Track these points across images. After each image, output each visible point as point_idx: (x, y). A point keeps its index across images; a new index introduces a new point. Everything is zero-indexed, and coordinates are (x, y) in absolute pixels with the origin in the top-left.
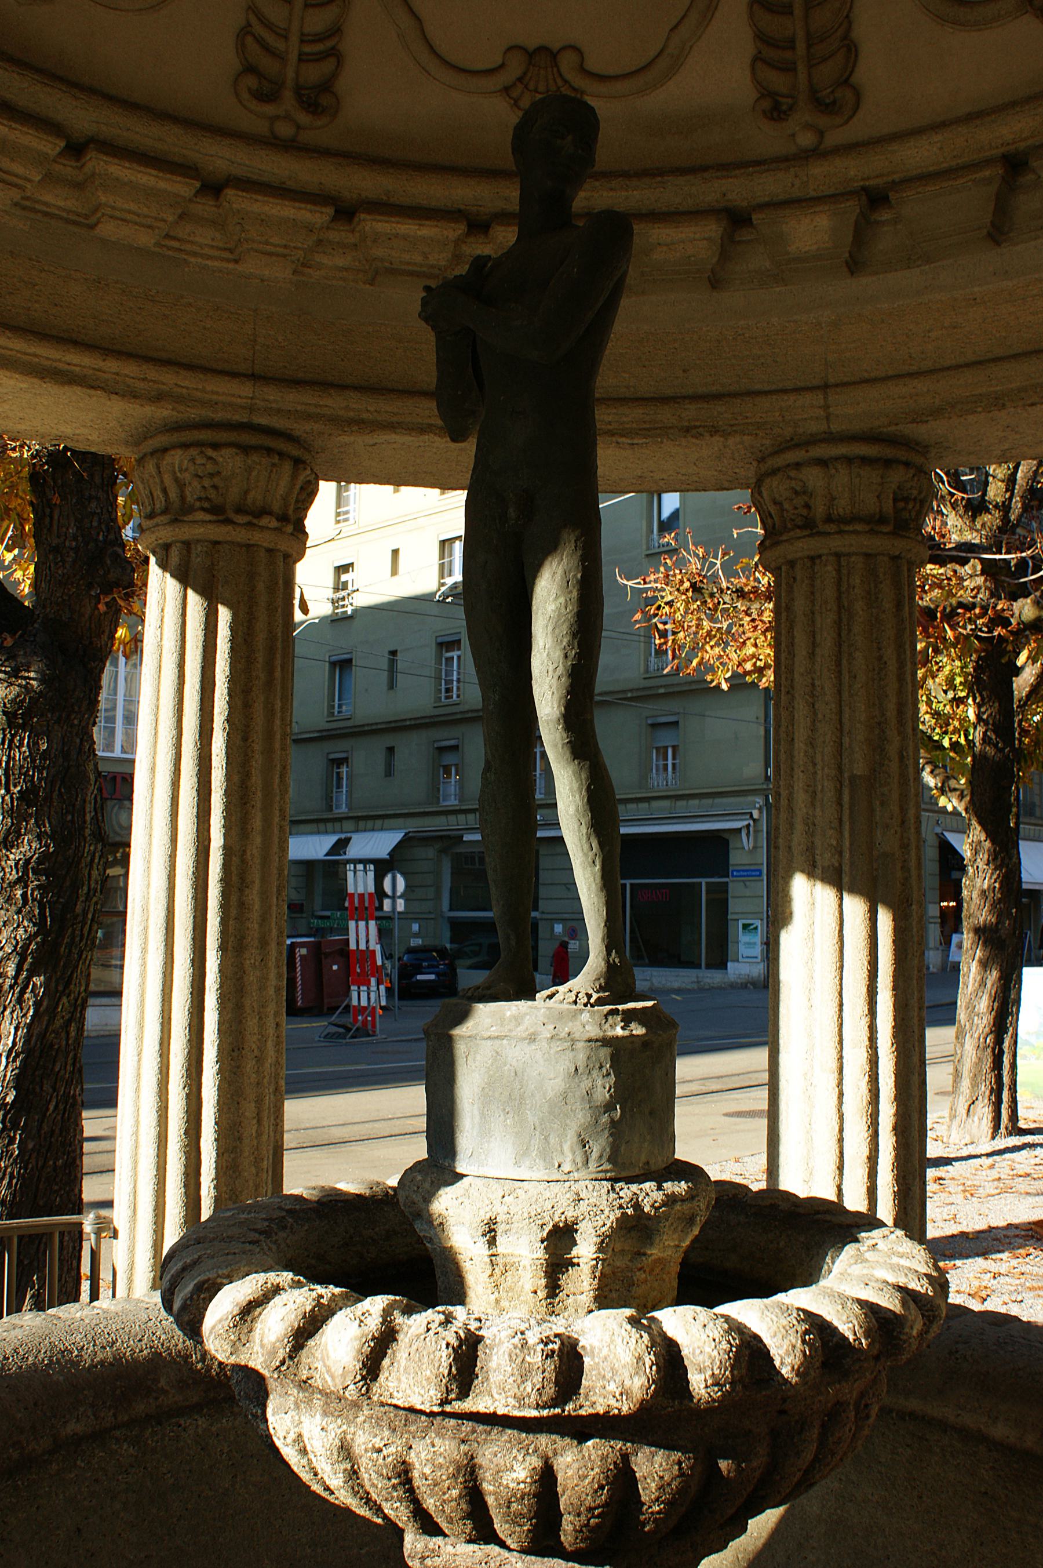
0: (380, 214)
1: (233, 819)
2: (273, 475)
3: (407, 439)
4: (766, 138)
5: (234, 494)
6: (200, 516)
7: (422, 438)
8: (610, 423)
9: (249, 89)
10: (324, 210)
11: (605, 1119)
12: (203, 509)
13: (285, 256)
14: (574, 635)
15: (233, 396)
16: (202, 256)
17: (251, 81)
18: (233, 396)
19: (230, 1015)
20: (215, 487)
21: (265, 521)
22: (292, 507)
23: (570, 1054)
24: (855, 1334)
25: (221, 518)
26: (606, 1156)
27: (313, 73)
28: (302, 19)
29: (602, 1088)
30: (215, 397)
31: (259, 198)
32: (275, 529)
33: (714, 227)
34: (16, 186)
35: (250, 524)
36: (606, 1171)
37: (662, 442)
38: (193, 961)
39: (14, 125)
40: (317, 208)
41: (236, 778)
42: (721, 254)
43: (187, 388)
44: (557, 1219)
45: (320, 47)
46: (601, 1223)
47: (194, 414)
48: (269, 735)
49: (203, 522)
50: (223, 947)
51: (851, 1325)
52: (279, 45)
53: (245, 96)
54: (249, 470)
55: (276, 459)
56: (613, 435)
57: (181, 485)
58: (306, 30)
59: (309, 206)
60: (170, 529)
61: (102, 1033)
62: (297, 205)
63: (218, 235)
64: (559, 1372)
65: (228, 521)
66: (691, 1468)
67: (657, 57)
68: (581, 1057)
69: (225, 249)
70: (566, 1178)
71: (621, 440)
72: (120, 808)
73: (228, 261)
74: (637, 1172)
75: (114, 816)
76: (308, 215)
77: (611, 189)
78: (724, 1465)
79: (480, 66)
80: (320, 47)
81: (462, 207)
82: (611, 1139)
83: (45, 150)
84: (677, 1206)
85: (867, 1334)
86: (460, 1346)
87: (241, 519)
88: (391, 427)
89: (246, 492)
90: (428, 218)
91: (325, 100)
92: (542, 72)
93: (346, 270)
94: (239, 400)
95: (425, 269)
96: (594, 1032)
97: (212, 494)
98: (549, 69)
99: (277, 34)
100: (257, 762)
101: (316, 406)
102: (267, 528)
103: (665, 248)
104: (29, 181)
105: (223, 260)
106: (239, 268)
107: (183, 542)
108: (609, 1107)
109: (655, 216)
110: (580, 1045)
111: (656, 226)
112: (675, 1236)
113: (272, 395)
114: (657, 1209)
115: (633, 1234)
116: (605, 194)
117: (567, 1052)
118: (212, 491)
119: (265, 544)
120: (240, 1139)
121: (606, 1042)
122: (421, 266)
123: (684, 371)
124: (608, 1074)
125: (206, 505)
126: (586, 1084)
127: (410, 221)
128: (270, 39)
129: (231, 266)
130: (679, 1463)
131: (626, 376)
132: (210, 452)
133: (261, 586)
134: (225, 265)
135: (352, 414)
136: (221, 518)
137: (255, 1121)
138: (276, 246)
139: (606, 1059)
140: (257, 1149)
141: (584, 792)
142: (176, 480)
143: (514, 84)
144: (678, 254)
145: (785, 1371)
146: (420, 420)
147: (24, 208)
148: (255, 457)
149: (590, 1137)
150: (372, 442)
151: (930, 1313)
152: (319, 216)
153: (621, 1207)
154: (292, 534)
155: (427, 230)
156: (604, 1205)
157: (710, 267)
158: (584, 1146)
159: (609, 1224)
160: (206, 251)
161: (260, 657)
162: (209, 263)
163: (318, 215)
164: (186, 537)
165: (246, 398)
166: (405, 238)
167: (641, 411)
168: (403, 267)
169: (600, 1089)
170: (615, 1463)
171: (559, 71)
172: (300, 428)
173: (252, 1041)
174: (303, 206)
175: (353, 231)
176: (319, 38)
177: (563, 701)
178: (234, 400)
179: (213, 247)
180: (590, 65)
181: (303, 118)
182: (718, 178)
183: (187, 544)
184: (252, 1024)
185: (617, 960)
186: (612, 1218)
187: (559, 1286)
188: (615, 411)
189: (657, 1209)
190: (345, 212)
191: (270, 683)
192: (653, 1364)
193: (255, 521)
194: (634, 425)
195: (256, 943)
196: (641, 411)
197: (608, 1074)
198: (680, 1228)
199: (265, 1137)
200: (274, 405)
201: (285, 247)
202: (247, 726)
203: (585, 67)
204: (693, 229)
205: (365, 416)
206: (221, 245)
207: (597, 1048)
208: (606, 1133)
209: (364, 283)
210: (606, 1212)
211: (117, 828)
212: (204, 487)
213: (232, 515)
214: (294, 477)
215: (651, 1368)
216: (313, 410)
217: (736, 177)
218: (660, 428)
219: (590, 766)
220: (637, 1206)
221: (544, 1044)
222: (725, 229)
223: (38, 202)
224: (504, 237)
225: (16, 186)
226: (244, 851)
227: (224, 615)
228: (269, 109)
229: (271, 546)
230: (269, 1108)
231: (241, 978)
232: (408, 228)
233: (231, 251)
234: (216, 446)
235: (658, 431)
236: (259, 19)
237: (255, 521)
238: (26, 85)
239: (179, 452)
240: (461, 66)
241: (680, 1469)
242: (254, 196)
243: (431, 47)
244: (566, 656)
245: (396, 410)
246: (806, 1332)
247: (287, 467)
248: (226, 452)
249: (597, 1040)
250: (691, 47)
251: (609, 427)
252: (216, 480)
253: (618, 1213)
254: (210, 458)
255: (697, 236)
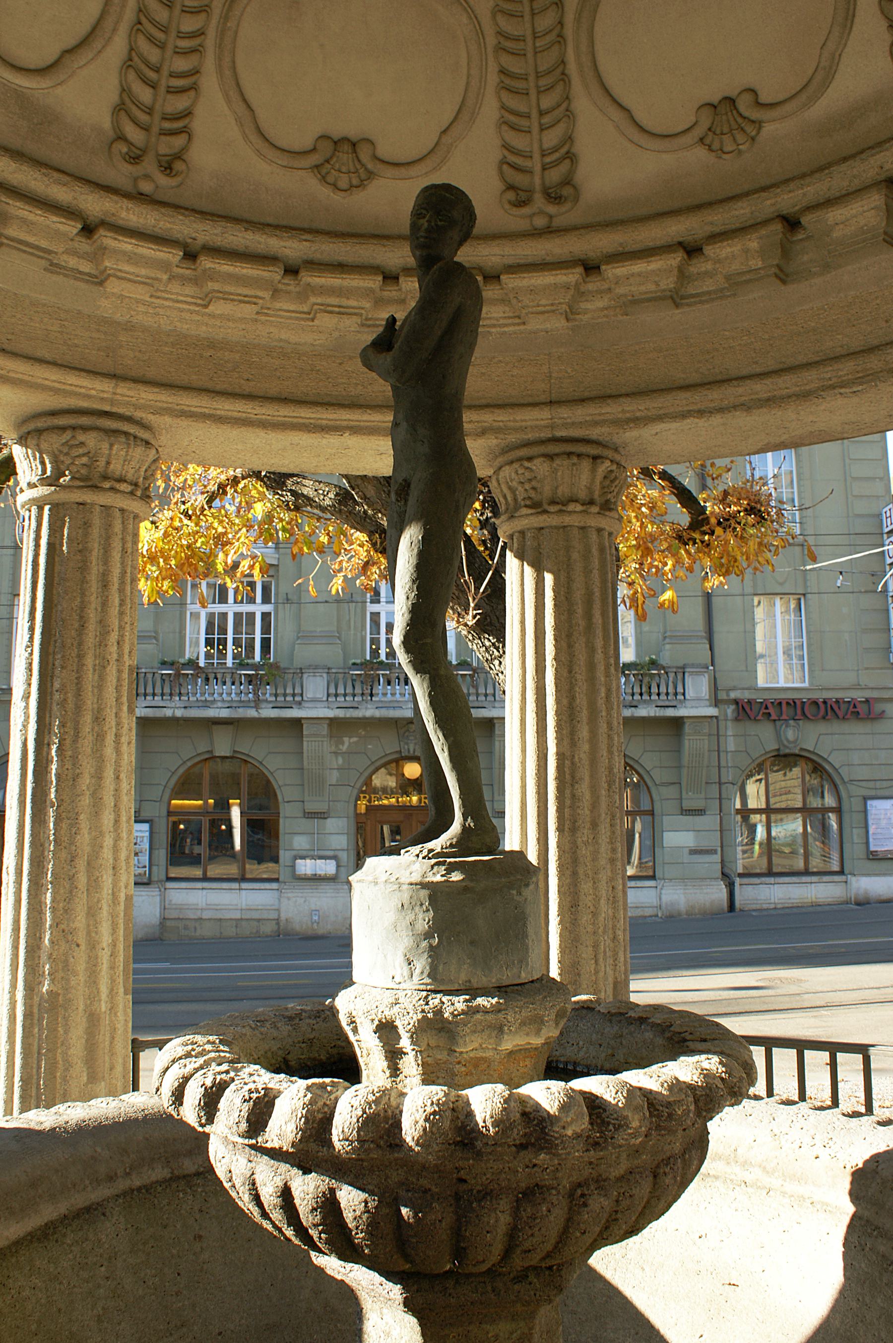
0: (617, 263)
1: (564, 732)
2: (574, 472)
3: (674, 425)
4: (516, 220)
5: (547, 491)
6: (525, 511)
7: (685, 422)
8: (830, 379)
9: (510, 202)
10: (574, 271)
11: (424, 944)
12: (526, 506)
13: (553, 311)
14: (414, 582)
15: (537, 420)
16: (500, 326)
17: (511, 195)
18: (537, 420)
19: (568, 881)
20: (534, 488)
21: (571, 507)
22: (597, 493)
23: (398, 894)
24: (484, 1122)
25: (539, 510)
26: (426, 972)
27: (555, 176)
28: (541, 140)
29: (423, 921)
30: (524, 424)
31: (525, 275)
32: (581, 512)
33: (877, 197)
34: (355, 314)
35: (561, 511)
36: (427, 984)
37: (876, 385)
38: (538, 839)
39: (344, 276)
40: (570, 271)
41: (565, 702)
42: (887, 218)
43: (502, 421)
44: (380, 1017)
45: (556, 155)
46: (406, 1022)
47: (512, 438)
48: (591, 667)
49: (527, 515)
50: (560, 829)
51: (484, 1114)
52: (527, 163)
53: (507, 206)
54: (555, 471)
55: (575, 460)
56: (834, 388)
57: (512, 490)
58: (545, 146)
59: (563, 272)
60: (507, 524)
61: (787, 905)
62: (554, 272)
63: (507, 309)
64: (251, 1113)
65: (545, 512)
66: (376, 1208)
67: (814, 74)
68: (406, 896)
69: (515, 317)
70: (397, 987)
71: (842, 391)
72: (787, 726)
73: (519, 324)
74: (456, 987)
75: (782, 733)
76: (564, 278)
77: (790, 192)
78: (404, 1211)
79: (680, 129)
80: (556, 155)
81: (681, 239)
82: (429, 960)
83: (369, 286)
84: (478, 1016)
85: (496, 1124)
86: (212, 1088)
87: (552, 509)
88: (660, 418)
89: (557, 488)
90: (652, 255)
91: (566, 191)
92: (724, 117)
93: (606, 309)
94: (542, 422)
95: (659, 294)
96: (416, 878)
97: (532, 494)
98: (729, 114)
99: (524, 156)
100: (581, 689)
101: (600, 414)
102: (575, 512)
103: (841, 226)
104: (363, 308)
105: (514, 325)
106: (528, 327)
107: (519, 532)
108: (428, 935)
109: (829, 202)
110: (405, 887)
111: (830, 210)
112: (492, 1041)
113: (565, 413)
114: (455, 1016)
115: (442, 1034)
116: (786, 197)
117: (396, 892)
118: (531, 491)
119: (576, 524)
120: (579, 974)
121: (424, 885)
122: (656, 292)
123: (887, 321)
124: (428, 910)
125: (528, 503)
126: (410, 917)
127: (639, 261)
128: (519, 161)
129: (522, 327)
130: (366, 1202)
131: (839, 337)
132: (526, 464)
133: (575, 555)
134: (517, 328)
135: (628, 415)
136: (539, 510)
137: (593, 962)
138: (544, 306)
139: (425, 898)
140: (595, 983)
141: (427, 698)
142: (510, 488)
143: (707, 134)
144: (853, 228)
145: (408, 1139)
146: (680, 409)
147: (369, 326)
148: (558, 461)
149: (414, 956)
150: (653, 432)
151: (616, 1122)
152: (573, 276)
153: (423, 1011)
154: (599, 513)
155: (655, 264)
156: (410, 1008)
157: (882, 231)
158: (410, 964)
159: (412, 1024)
160: (501, 321)
161: (580, 610)
162: (506, 329)
163: (571, 276)
164: (519, 528)
165: (547, 419)
166: (639, 274)
167: (853, 364)
168: (643, 297)
169: (421, 921)
170: (324, 1193)
171: (738, 112)
172: (594, 433)
173: (587, 900)
174: (558, 272)
175: (604, 280)
176: (555, 149)
177: (403, 632)
178: (538, 423)
179: (505, 318)
180: (764, 98)
181: (552, 209)
182: (872, 155)
183: (522, 533)
184: (586, 887)
185: (472, 825)
186: (415, 1019)
187: (399, 1069)
188: (831, 368)
189: (455, 1016)
190: (591, 268)
191: (589, 627)
192: (302, 1116)
193: (564, 508)
194: (850, 377)
195: (588, 825)
196: (853, 364)
197: (428, 910)
198: (493, 1035)
199: (601, 974)
200: (569, 421)
201: (552, 305)
202: (571, 662)
203: (760, 101)
204: (860, 204)
205: (638, 414)
206: (511, 315)
207: (418, 890)
208: (426, 955)
209: (622, 315)
210: (411, 1015)
211: (786, 743)
212: (526, 490)
213: (546, 507)
214: (593, 471)
215: (300, 1120)
216: (598, 418)
217: (887, 150)
218: (872, 374)
219: (430, 678)
220: (438, 1012)
221: (382, 886)
222: (886, 195)
223: (377, 319)
224: (714, 253)
225: (355, 314)
226: (573, 756)
227: (549, 578)
228: (526, 210)
229: (582, 524)
230: (605, 952)
231: (575, 852)
232: (639, 267)
233: (519, 317)
234: (530, 459)
235: (871, 377)
236: (509, 151)
237: (564, 508)
238: (349, 248)
239: (507, 467)
240: (665, 133)
241: (366, 1206)
242: (522, 275)
243: (640, 127)
244: (408, 598)
245: (660, 405)
246: (434, 1113)
247: (586, 464)
248: (537, 461)
249: (416, 884)
250: (840, 55)
251: (830, 382)
252: (534, 483)
253: (420, 1016)
254: (527, 468)
255: (865, 208)
